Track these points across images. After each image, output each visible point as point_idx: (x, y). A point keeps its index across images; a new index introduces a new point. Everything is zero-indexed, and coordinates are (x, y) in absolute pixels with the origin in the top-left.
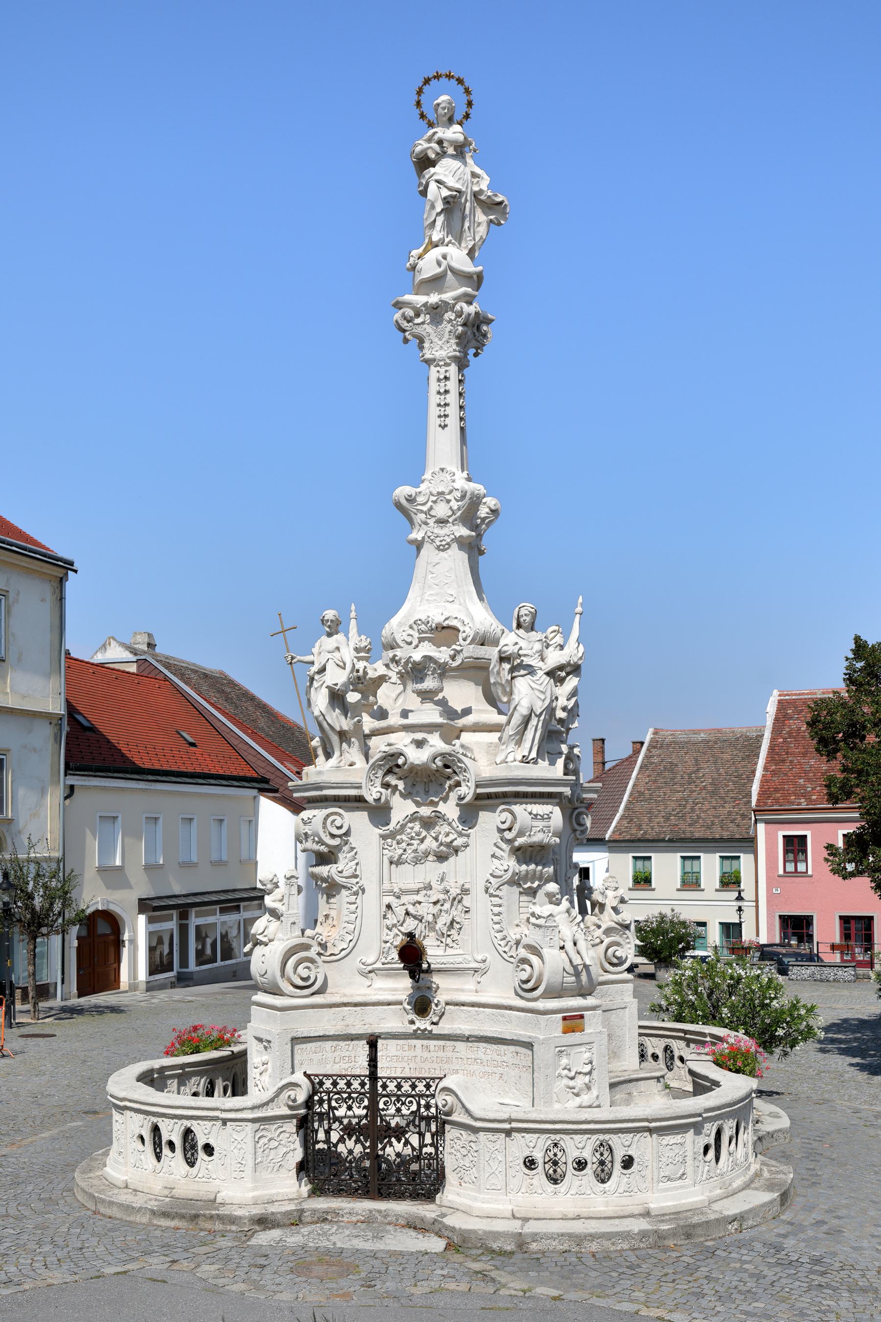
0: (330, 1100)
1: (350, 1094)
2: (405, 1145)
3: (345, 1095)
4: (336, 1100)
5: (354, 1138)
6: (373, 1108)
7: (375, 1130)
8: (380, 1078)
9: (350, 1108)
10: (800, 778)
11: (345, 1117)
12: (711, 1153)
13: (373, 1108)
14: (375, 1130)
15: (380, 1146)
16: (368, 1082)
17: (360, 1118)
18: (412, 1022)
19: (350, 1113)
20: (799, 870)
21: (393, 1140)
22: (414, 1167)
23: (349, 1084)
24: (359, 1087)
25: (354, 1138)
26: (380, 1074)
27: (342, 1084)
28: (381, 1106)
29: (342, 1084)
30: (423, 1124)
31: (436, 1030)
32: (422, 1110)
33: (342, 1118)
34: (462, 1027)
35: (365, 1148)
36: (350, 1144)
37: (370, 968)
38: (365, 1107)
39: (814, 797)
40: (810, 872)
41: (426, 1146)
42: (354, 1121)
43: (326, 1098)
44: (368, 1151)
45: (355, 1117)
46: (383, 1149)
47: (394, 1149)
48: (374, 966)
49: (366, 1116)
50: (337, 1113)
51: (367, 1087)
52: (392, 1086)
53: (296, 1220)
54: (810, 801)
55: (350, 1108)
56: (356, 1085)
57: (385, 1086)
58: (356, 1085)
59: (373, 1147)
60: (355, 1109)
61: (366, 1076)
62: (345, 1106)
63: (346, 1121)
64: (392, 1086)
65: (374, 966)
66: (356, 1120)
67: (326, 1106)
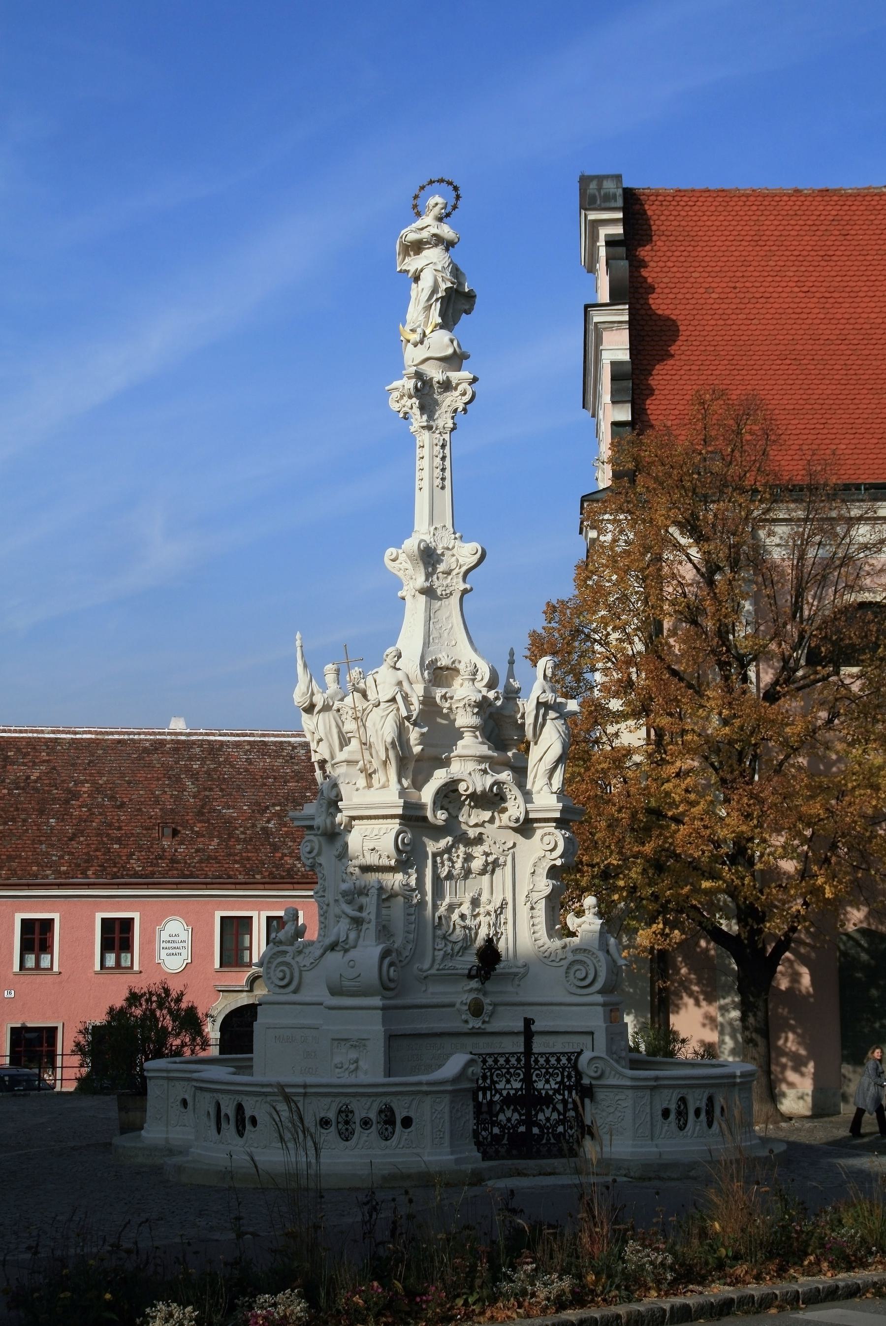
0: (492, 1075)
1: (508, 1069)
2: (553, 1111)
3: (504, 1071)
4: (498, 1075)
5: (512, 1107)
6: (528, 1081)
7: (529, 1100)
8: (534, 1054)
9: (508, 1082)
10: (41, 843)
11: (505, 1089)
12: (703, 1116)
13: (528, 1081)
14: (529, 1100)
15: (533, 1113)
16: (523, 1059)
17: (516, 1090)
18: (466, 1022)
19: (508, 1086)
20: (123, 964)
21: (544, 1107)
22: (560, 1129)
23: (507, 1061)
24: (516, 1063)
25: (512, 1107)
26: (535, 1050)
27: (502, 1061)
28: (534, 1078)
29: (502, 1061)
30: (566, 1093)
31: (489, 1028)
32: (566, 1080)
33: (502, 1090)
34: (511, 1024)
35: (520, 1115)
36: (509, 1113)
37: (425, 974)
38: (520, 1081)
39: (63, 869)
40: (136, 968)
41: (569, 1110)
42: (512, 1092)
43: (489, 1074)
44: (523, 1117)
45: (512, 1089)
46: (536, 1115)
47: (545, 1115)
48: (429, 972)
49: (521, 1089)
50: (498, 1086)
51: (523, 1062)
52: (542, 1061)
53: (477, 1178)
54: (59, 874)
55: (508, 1082)
56: (513, 1061)
57: (536, 1061)
58: (513, 1061)
59: (529, 1114)
60: (513, 1082)
61: (521, 1053)
62: (504, 1079)
63: (505, 1093)
64: (542, 1061)
65: (429, 972)
66: (514, 1092)
67: (488, 1081)
